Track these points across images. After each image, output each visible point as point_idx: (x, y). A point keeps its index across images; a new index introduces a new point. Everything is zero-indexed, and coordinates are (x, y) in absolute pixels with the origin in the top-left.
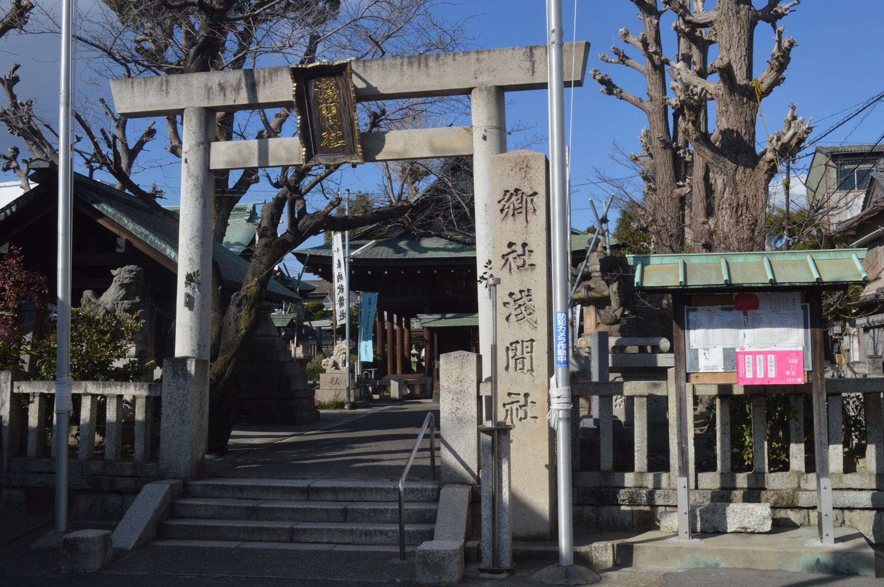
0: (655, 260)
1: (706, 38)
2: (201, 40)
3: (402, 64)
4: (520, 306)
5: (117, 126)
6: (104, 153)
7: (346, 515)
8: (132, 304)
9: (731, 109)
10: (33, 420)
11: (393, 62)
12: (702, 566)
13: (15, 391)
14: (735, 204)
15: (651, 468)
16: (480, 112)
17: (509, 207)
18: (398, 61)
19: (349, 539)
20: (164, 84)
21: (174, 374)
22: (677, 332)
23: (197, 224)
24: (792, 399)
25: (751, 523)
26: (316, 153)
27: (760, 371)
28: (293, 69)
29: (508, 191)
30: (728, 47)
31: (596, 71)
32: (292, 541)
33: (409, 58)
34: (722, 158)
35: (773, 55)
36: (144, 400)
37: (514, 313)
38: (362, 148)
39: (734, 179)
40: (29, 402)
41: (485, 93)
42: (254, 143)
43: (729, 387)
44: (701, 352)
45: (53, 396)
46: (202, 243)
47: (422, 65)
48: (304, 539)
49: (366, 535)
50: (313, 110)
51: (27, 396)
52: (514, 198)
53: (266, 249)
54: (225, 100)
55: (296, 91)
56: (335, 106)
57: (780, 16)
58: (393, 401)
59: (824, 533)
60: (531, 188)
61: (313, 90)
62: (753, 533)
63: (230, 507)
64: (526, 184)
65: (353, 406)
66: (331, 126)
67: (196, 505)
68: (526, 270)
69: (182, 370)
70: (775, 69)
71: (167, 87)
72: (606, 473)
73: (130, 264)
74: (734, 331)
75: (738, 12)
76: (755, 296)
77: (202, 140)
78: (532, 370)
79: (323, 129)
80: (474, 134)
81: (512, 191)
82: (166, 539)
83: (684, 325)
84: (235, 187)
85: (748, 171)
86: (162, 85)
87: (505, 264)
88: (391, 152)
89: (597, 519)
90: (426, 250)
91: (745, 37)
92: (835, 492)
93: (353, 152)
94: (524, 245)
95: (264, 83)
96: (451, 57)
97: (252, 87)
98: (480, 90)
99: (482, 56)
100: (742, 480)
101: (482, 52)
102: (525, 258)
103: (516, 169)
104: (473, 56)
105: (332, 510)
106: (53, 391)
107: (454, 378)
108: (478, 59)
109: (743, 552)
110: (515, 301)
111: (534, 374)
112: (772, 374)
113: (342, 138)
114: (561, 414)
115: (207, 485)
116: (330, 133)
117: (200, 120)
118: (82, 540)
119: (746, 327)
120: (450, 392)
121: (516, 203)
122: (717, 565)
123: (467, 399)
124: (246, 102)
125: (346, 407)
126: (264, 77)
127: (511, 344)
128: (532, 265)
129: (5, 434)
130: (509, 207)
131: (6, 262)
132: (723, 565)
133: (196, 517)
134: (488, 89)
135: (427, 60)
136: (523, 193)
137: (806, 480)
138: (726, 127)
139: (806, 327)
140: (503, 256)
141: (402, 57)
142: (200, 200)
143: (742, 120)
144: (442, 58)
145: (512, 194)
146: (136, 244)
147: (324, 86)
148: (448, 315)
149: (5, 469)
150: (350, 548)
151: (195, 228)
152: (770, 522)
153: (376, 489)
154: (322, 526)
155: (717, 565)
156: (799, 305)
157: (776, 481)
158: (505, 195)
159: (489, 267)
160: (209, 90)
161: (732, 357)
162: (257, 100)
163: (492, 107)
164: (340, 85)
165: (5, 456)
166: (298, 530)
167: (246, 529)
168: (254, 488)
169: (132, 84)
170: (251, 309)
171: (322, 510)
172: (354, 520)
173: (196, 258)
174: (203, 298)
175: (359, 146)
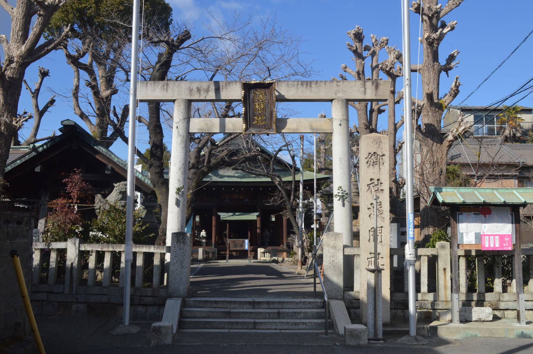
0: (444, 190)
1: (395, 74)
3: (298, 85)
5: (33, 97)
6: (112, 119)
7: (279, 315)
9: (430, 114)
11: (293, 83)
12: (469, 336)
14: (432, 162)
15: (429, 291)
18: (296, 83)
19: (286, 327)
20: (166, 86)
22: (454, 225)
23: (182, 162)
24: (496, 258)
25: (483, 317)
27: (491, 244)
28: (244, 84)
32: (255, 329)
35: (452, 89)
39: (432, 149)
41: (341, 102)
42: (217, 121)
43: (470, 251)
44: (464, 234)
47: (308, 86)
48: (261, 327)
49: (295, 325)
51: (89, 252)
52: (373, 157)
57: (451, 69)
59: (521, 320)
61: (252, 95)
62: (483, 321)
63: (215, 312)
66: (260, 114)
67: (195, 311)
68: (379, 192)
70: (452, 95)
74: (481, 224)
75: (433, 66)
76: (489, 208)
78: (381, 242)
79: (254, 115)
81: (372, 153)
82: (183, 329)
83: (457, 221)
84: (111, 136)
85: (438, 145)
86: (164, 86)
88: (290, 129)
89: (404, 316)
90: (222, 177)
91: (436, 78)
92: (526, 302)
93: (270, 128)
94: (378, 180)
95: (222, 89)
96: (323, 83)
97: (217, 90)
98: (338, 101)
99: (339, 84)
100: (475, 297)
102: (379, 186)
103: (375, 143)
105: (272, 313)
109: (489, 329)
111: (383, 243)
112: (497, 245)
113: (265, 120)
115: (196, 301)
116: (258, 117)
118: (163, 327)
119: (485, 222)
122: (476, 336)
124: (214, 98)
126: (223, 86)
128: (382, 190)
132: (479, 335)
133: (195, 318)
134: (342, 100)
137: (503, 296)
138: (427, 122)
139: (512, 223)
140: (368, 185)
141: (298, 81)
142: (184, 148)
143: (435, 120)
146: (116, 169)
147: (258, 93)
148: (237, 214)
149: (74, 293)
150: (288, 331)
151: (181, 163)
152: (492, 316)
153: (291, 302)
154: (267, 321)
155: (476, 336)
156: (509, 213)
157: (489, 296)
160: (191, 90)
161: (479, 237)
163: (344, 108)
164: (267, 94)
166: (258, 323)
167: (229, 323)
168: (223, 302)
170: (189, 207)
171: (266, 312)
172: (284, 318)
173: (182, 180)
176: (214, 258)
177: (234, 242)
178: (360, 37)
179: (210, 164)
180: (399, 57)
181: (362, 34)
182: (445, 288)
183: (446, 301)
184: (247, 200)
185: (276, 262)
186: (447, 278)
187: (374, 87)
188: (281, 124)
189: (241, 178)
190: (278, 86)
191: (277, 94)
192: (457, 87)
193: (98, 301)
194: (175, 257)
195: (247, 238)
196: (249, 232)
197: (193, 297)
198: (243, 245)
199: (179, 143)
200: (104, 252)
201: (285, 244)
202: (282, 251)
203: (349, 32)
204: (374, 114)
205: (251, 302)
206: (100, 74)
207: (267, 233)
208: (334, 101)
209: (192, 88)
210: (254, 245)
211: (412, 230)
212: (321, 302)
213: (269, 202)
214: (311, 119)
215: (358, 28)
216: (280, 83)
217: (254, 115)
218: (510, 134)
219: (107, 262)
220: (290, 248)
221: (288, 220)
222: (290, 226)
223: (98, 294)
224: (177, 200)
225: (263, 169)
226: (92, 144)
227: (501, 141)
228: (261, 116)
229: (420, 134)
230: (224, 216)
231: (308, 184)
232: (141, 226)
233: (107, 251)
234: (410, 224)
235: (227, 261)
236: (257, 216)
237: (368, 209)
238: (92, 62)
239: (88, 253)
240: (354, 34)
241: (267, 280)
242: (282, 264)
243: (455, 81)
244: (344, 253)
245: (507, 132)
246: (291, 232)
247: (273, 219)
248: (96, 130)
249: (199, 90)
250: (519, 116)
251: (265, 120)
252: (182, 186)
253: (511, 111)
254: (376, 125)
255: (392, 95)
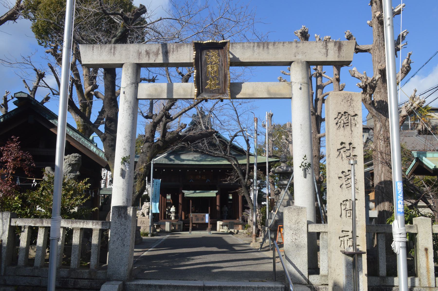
2: (119, 34)
3: (254, 46)
4: (348, 179)
8: (75, 175)
10: (23, 243)
11: (248, 45)
13: (12, 224)
16: (297, 75)
17: (340, 122)
18: (252, 45)
20: (113, 49)
21: (119, 216)
26: (202, 92)
28: (195, 43)
29: (339, 113)
30: (379, 61)
31: (281, 78)
33: (258, 43)
34: (380, 114)
36: (98, 232)
37: (345, 183)
38: (230, 90)
40: (21, 232)
41: (300, 64)
45: (49, 227)
46: (131, 140)
47: (265, 48)
50: (203, 67)
51: (20, 227)
52: (343, 117)
53: (149, 148)
54: (149, 60)
55: (196, 56)
56: (216, 66)
58: (167, 233)
60: (354, 112)
61: (204, 57)
64: (351, 109)
65: (153, 235)
66: (213, 77)
69: (124, 213)
70: (404, 72)
71: (114, 50)
72: (383, 278)
73: (75, 153)
77: (134, 81)
79: (207, 79)
80: (293, 87)
81: (343, 113)
86: (111, 49)
87: (339, 154)
88: (245, 94)
93: (223, 93)
94: (350, 144)
95: (173, 52)
96: (282, 44)
97: (166, 54)
98: (298, 63)
99: (299, 45)
101: (299, 42)
102: (351, 151)
104: (294, 44)
106: (50, 225)
107: (294, 221)
108: (297, 46)
110: (345, 176)
113: (218, 84)
114: (401, 244)
115: (138, 285)
117: (133, 70)
120: (291, 229)
121: (345, 120)
123: (301, 234)
125: (149, 235)
126: (173, 49)
127: (343, 201)
128: (355, 156)
129: (4, 251)
130: (340, 122)
131: (8, 146)
135: (268, 44)
136: (349, 114)
138: (379, 99)
142: (131, 115)
144: (276, 44)
145: (342, 115)
146: (72, 143)
148: (197, 191)
149: (2, 274)
151: (128, 131)
153: (247, 287)
158: (338, 115)
159: (305, 158)
160: (139, 54)
162: (168, 61)
164: (221, 55)
165: (3, 265)
169: (93, 48)
170: (142, 181)
173: (128, 149)
174: (130, 172)
175: (229, 89)
176: (179, 230)
177: (196, 216)
178: (306, 36)
179: (165, 138)
180: (350, 37)
181: (307, 33)
182: (428, 271)
183: (430, 287)
184: (208, 180)
185: (231, 233)
186: (429, 260)
187: (336, 48)
188: (235, 88)
189: (201, 161)
190: (232, 48)
191: (231, 56)
192: (409, 63)
193: (28, 284)
194: (115, 233)
195: (207, 213)
196: (209, 208)
197: (137, 279)
198: (203, 219)
199: (125, 109)
200: (37, 228)
201: (240, 218)
202: (238, 224)
203: (296, 31)
204: (319, 103)
205: (201, 287)
206: (84, 73)
207: (226, 209)
208: (293, 64)
209: (140, 51)
210: (214, 220)
211: (402, 202)
212: (282, 288)
213: (226, 181)
214: (268, 83)
215: (304, 28)
216: (234, 45)
217: (207, 79)
218: (422, 128)
219: (40, 241)
220: (245, 222)
221: (243, 197)
222: (245, 202)
223: (29, 276)
224: (122, 170)
225: (221, 152)
226: (47, 118)
227: (417, 134)
228: (214, 80)
229: (374, 110)
230: (188, 193)
231: (261, 166)
232: (82, 199)
233: (41, 227)
234: (398, 195)
235: (190, 233)
236: (217, 194)
237: (339, 178)
238: (76, 61)
239: (19, 229)
240: (301, 33)
241: (222, 255)
242: (237, 235)
243: (408, 57)
244: (308, 230)
245: (420, 127)
246: (245, 207)
247: (231, 197)
248: (80, 120)
249: (148, 53)
250: (429, 114)
251: (218, 84)
252: (128, 156)
253: (423, 110)
254: (321, 112)
255: (337, 83)
